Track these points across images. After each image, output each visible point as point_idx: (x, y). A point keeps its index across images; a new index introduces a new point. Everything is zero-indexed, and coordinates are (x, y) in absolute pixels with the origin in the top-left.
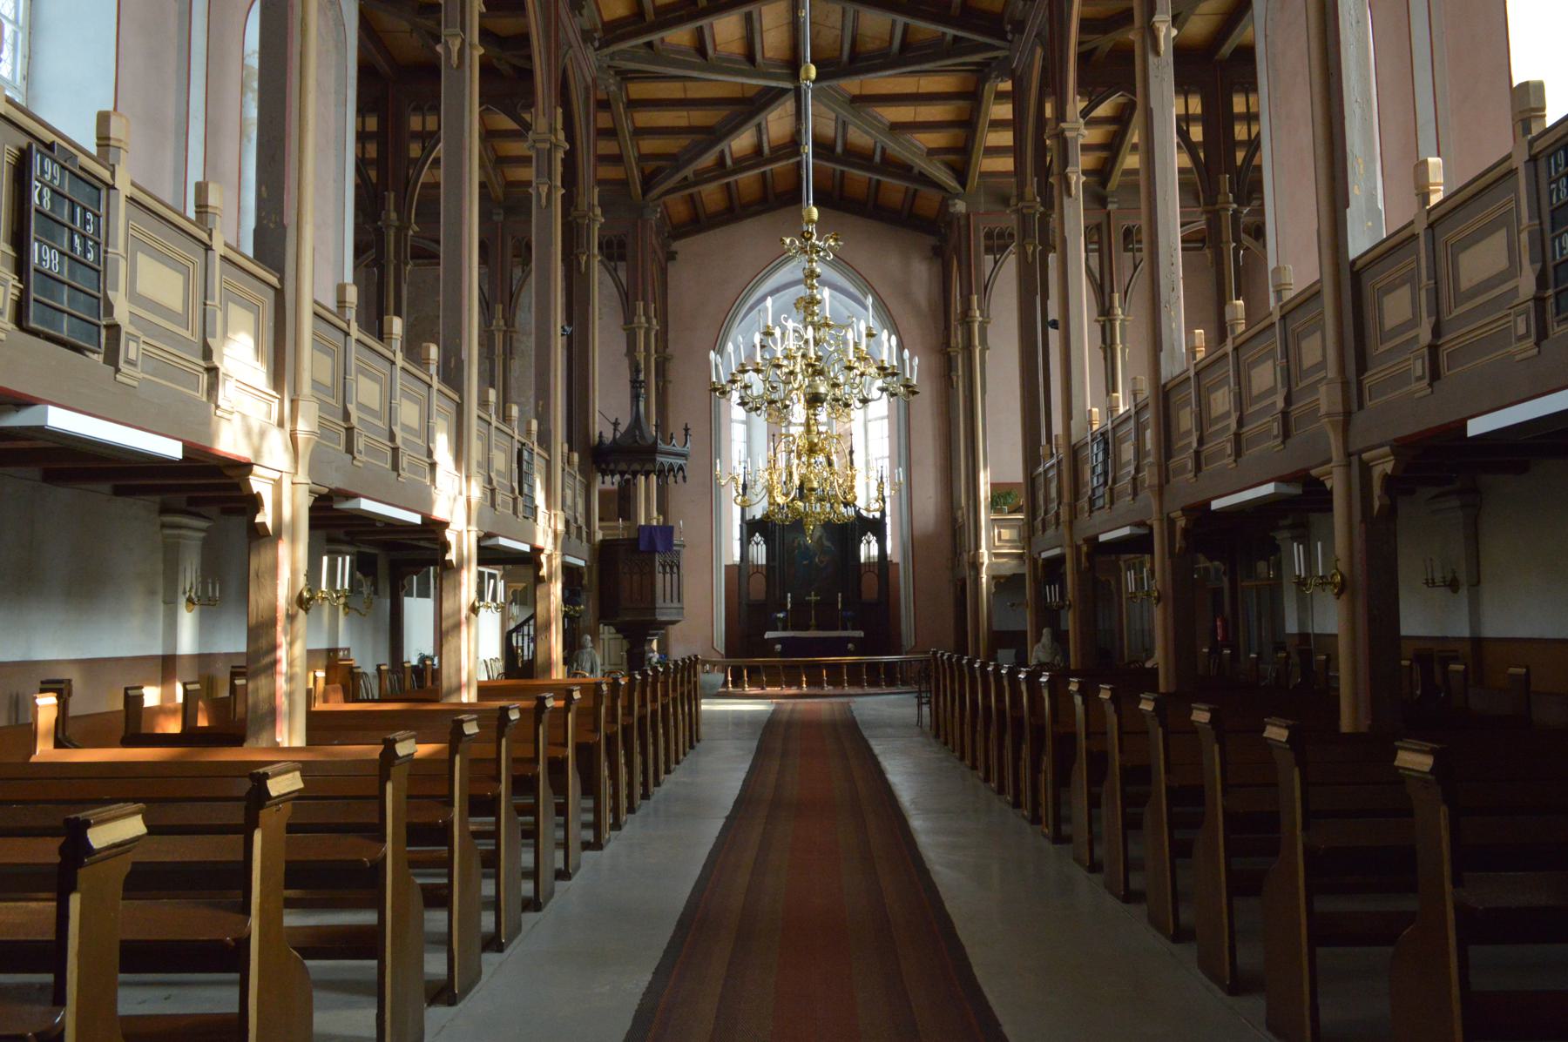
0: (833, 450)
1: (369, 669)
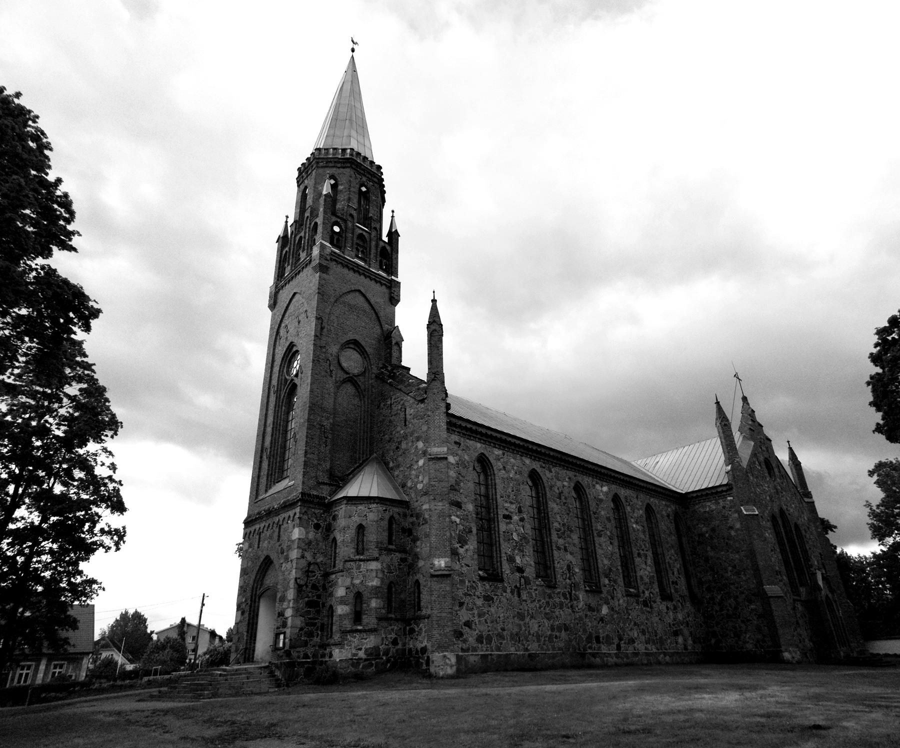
0: (673, 591)
1: (739, 697)
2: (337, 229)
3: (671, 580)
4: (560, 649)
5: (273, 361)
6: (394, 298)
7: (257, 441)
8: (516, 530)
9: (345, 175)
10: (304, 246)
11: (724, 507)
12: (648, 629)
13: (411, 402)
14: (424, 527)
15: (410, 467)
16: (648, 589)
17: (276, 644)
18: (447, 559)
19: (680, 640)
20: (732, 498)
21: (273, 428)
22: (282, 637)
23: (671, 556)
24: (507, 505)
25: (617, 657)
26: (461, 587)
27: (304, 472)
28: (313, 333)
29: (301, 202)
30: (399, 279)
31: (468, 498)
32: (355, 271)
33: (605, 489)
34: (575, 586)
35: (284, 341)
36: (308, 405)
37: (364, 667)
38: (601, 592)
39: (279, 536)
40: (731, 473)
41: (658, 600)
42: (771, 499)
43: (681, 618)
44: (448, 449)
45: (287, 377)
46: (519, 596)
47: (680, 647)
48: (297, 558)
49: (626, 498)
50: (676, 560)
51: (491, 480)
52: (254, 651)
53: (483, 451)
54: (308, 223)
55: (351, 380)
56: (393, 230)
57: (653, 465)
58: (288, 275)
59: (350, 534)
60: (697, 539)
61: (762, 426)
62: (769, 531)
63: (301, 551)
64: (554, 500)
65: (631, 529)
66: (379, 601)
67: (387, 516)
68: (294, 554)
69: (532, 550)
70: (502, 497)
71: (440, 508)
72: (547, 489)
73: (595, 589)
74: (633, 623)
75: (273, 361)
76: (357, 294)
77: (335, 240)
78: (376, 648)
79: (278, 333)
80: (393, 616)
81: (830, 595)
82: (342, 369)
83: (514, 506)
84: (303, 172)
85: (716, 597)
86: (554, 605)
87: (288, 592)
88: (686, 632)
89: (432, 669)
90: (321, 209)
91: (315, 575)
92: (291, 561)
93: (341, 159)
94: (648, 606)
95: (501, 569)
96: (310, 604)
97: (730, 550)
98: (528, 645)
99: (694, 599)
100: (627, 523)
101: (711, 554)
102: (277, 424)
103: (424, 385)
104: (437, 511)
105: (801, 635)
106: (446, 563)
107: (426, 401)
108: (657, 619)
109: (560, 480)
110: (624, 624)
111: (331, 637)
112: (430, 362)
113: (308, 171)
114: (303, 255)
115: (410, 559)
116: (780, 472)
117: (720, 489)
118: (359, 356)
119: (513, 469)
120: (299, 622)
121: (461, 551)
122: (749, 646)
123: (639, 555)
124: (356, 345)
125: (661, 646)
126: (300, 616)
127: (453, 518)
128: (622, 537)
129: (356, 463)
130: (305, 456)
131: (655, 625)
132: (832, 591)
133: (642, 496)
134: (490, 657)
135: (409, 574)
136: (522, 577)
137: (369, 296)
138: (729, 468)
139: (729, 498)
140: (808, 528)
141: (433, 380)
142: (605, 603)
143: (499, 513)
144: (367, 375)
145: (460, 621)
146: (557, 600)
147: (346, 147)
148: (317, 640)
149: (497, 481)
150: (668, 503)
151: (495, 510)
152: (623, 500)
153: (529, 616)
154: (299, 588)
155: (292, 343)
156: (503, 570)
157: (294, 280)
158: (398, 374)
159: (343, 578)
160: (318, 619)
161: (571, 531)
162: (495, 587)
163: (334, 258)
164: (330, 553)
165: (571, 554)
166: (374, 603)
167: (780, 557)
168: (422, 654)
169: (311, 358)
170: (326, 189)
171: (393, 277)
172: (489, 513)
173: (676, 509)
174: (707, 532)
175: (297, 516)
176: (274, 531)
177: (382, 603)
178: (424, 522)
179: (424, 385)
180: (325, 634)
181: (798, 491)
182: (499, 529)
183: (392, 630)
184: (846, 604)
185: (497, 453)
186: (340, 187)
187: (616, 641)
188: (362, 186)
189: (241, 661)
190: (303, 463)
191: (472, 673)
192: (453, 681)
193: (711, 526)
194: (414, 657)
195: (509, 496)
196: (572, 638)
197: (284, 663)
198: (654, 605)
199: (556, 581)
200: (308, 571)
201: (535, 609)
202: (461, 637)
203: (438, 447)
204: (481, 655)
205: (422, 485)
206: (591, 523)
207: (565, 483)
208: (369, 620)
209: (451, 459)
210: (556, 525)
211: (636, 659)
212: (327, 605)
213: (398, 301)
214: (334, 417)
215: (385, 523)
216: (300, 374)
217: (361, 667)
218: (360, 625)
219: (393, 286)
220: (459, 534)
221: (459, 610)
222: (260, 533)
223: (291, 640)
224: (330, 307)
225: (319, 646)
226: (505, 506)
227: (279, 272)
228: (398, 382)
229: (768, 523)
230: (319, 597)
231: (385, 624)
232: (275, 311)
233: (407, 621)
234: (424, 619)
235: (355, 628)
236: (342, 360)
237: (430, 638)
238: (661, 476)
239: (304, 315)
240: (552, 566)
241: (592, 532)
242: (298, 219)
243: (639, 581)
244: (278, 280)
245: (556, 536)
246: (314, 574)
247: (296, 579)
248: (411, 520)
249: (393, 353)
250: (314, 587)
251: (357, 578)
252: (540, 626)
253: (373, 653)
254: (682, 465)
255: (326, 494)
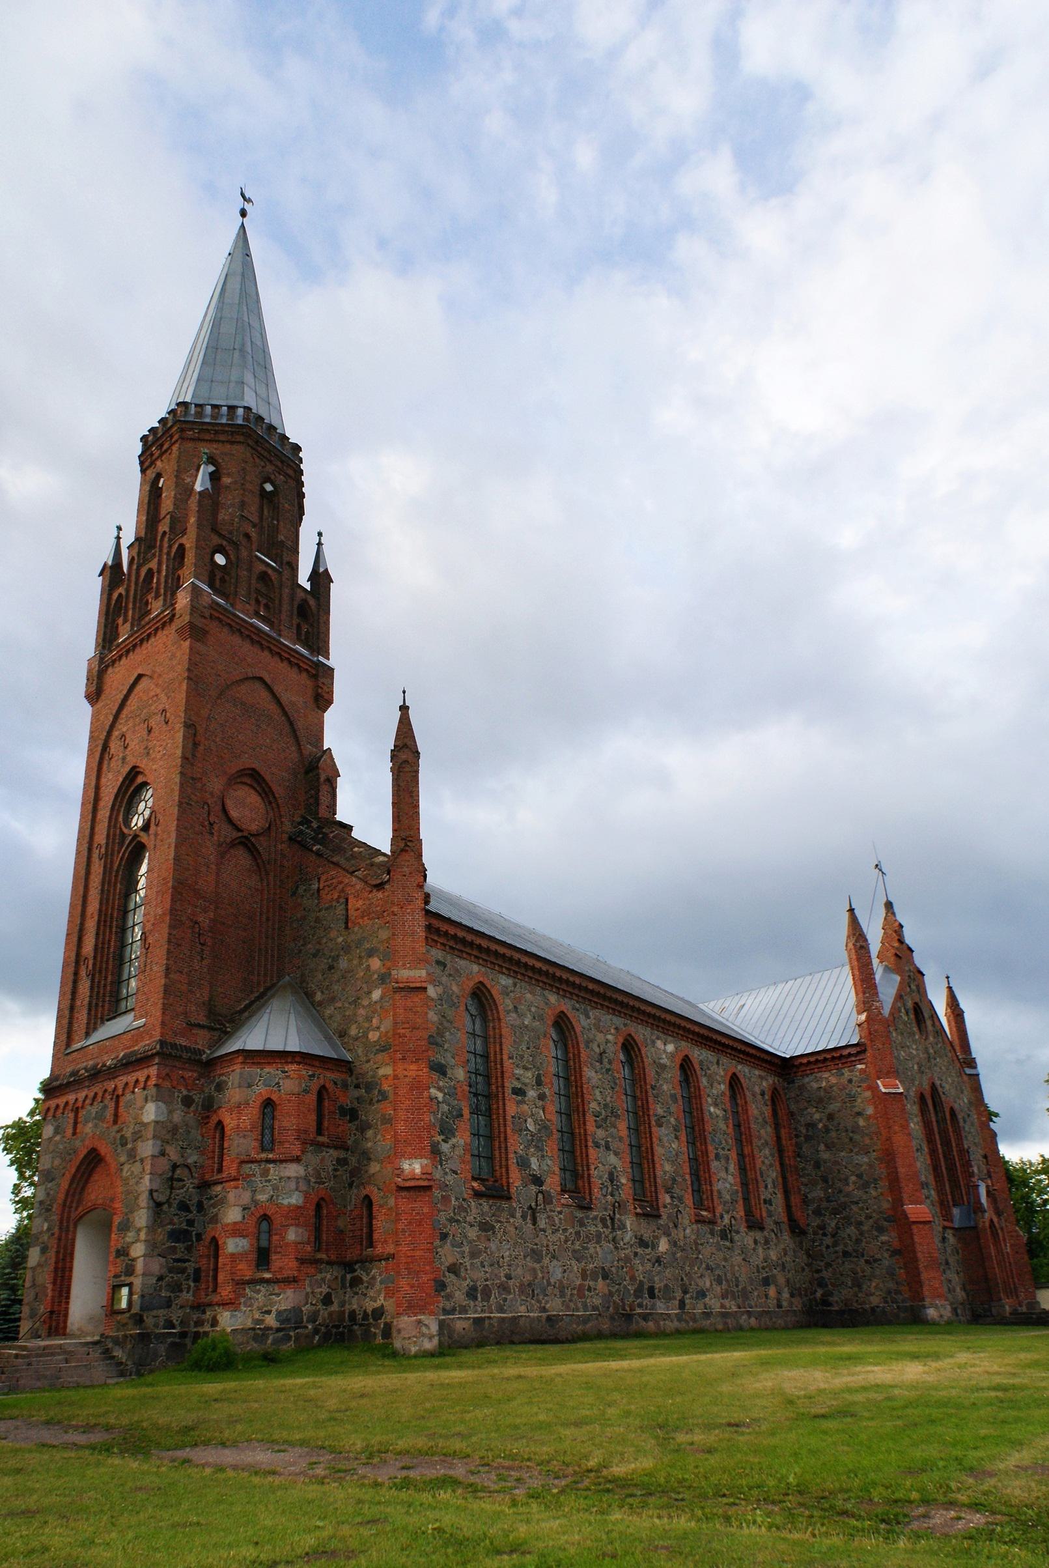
0: (764, 1214)
2: (220, 559)
3: (763, 1197)
4: (595, 1308)
5: (97, 799)
6: (322, 697)
7: (67, 944)
8: (533, 1115)
9: (236, 455)
10: (158, 589)
11: (850, 1081)
12: (726, 1275)
13: (358, 887)
14: (381, 1106)
15: (356, 1002)
16: (728, 1212)
17: (112, 1304)
18: (425, 1161)
19: (772, 1291)
20: (863, 1066)
21: (99, 921)
22: (125, 1291)
23: (765, 1157)
24: (518, 1071)
25: (679, 1320)
26: (443, 1208)
27: (164, 1004)
28: (179, 752)
29: (149, 502)
30: (332, 662)
31: (457, 1058)
32: (252, 641)
33: (670, 1048)
34: (619, 1206)
35: (120, 762)
36: (170, 884)
37: (275, 1342)
38: (659, 1216)
39: (116, 1115)
40: (865, 1025)
41: (743, 1229)
42: (920, 1068)
43: (774, 1258)
44: (428, 974)
45: (126, 831)
46: (534, 1222)
47: (772, 1303)
48: (153, 1156)
49: (701, 1063)
50: (771, 1165)
51: (494, 1028)
52: (66, 1315)
53: (481, 979)
54: (166, 545)
55: (246, 842)
56: (321, 570)
57: (735, 1012)
58: (126, 639)
59: (248, 1118)
60: (804, 1131)
61: (912, 951)
62: (915, 1120)
63: (159, 1142)
64: (591, 1064)
65: (707, 1117)
66: (300, 1230)
67: (315, 1086)
68: (147, 1148)
69: (555, 1147)
70: (510, 1058)
71: (414, 1074)
72: (582, 1046)
73: (651, 1214)
74: (704, 1266)
75: (97, 799)
76: (258, 685)
77: (214, 576)
78: (296, 1311)
79: (105, 747)
80: (324, 1256)
81: (995, 1220)
82: (230, 821)
83: (529, 1074)
84: (151, 446)
85: (829, 1224)
86: (587, 1236)
87: (135, 1214)
88: (781, 1280)
89: (398, 1344)
90: (192, 520)
91: (185, 1185)
92: (142, 1160)
93: (226, 424)
94: (727, 1239)
95: (508, 1178)
96: (178, 1236)
97: (855, 1150)
98: (547, 1302)
99: (796, 1229)
100: (701, 1104)
101: (826, 1156)
102: (106, 915)
103: (381, 858)
104: (407, 1080)
105: (950, 1281)
106: (422, 1167)
107: (387, 886)
108: (739, 1259)
109: (602, 1032)
110: (692, 1266)
111: (215, 1291)
112: (397, 818)
113: (161, 446)
114: (156, 607)
115: (353, 1161)
116: (933, 1025)
117: (845, 1052)
118: (259, 799)
119: (530, 1011)
120: (157, 1266)
121: (445, 1147)
122: (875, 1300)
123: (717, 1157)
124: (254, 778)
125: (744, 1302)
126: (159, 1255)
127: (433, 1091)
128: (693, 1128)
129: (252, 992)
130: (167, 976)
131: (737, 1268)
132: (999, 1213)
133: (724, 1060)
134: (487, 1322)
135: (351, 1185)
136: (539, 1192)
137: (278, 689)
138: (863, 1017)
139: (859, 1067)
140: (969, 1115)
141: (402, 850)
142: (664, 1234)
143: (506, 1084)
144: (273, 834)
145: (441, 1264)
146: (593, 1229)
147: (235, 403)
148: (187, 1296)
149: (504, 1031)
150: (763, 1074)
151: (500, 1079)
152: (697, 1067)
153: (549, 1256)
154: (157, 1207)
155: (134, 767)
156: (511, 1181)
157: (138, 650)
158: (332, 835)
159: (237, 1191)
160: (188, 1261)
161: (617, 1117)
162: (498, 1209)
163: (217, 615)
164: (210, 1148)
165: (616, 1154)
166: (292, 1235)
167: (929, 1162)
168: (375, 1319)
169: (177, 798)
170: (201, 483)
171: (321, 659)
172: (489, 1084)
173: (774, 1083)
174: (820, 1120)
175: (153, 1081)
176: (105, 1107)
177: (306, 1234)
178: (380, 1098)
179: (381, 858)
180: (203, 1286)
181: (957, 1056)
182: (504, 1111)
183: (323, 1279)
184: (1014, 1234)
185: (503, 983)
186: (226, 480)
187: (678, 1294)
188: (265, 482)
189: (43, 1333)
190: (162, 989)
191: (460, 1347)
192: (437, 1361)
193: (827, 1111)
194: (361, 1325)
195: (522, 1057)
196: (614, 1290)
197: (131, 1335)
198: (736, 1238)
199: (591, 1199)
200: (172, 1179)
201: (558, 1243)
202: (443, 1290)
203: (409, 969)
204: (474, 1318)
205: (378, 1034)
206: (647, 1102)
207: (610, 1037)
208: (283, 1263)
209: (432, 991)
210: (593, 1105)
211: (706, 1323)
212: (207, 1238)
213: (330, 702)
214: (217, 908)
215: (312, 1097)
216: (153, 828)
217: (269, 1341)
218: (268, 1270)
219: (321, 674)
220: (442, 1118)
221: (441, 1247)
222: (77, 1108)
223: (143, 1296)
224: (209, 706)
225: (192, 1307)
226: (518, 1074)
227: (105, 633)
228: (333, 851)
229: (914, 1107)
230: (190, 1223)
231: (311, 1270)
232: (100, 704)
233: (349, 1266)
234: (380, 1260)
235: (259, 1275)
236: (230, 804)
237: (389, 1294)
238: (749, 1029)
239: (159, 718)
240: (586, 1172)
241: (649, 1119)
242: (143, 534)
243: (715, 1198)
244: (104, 647)
245: (594, 1124)
246: (181, 1183)
247: (151, 1192)
248: (356, 1093)
249: (321, 797)
250: (184, 1207)
251: (263, 1191)
252: (565, 1271)
253: (291, 1320)
254: (783, 1012)
255: (202, 1045)
